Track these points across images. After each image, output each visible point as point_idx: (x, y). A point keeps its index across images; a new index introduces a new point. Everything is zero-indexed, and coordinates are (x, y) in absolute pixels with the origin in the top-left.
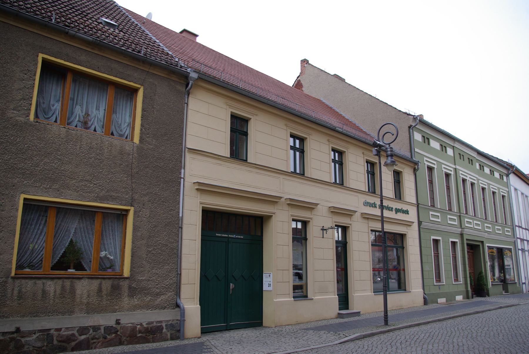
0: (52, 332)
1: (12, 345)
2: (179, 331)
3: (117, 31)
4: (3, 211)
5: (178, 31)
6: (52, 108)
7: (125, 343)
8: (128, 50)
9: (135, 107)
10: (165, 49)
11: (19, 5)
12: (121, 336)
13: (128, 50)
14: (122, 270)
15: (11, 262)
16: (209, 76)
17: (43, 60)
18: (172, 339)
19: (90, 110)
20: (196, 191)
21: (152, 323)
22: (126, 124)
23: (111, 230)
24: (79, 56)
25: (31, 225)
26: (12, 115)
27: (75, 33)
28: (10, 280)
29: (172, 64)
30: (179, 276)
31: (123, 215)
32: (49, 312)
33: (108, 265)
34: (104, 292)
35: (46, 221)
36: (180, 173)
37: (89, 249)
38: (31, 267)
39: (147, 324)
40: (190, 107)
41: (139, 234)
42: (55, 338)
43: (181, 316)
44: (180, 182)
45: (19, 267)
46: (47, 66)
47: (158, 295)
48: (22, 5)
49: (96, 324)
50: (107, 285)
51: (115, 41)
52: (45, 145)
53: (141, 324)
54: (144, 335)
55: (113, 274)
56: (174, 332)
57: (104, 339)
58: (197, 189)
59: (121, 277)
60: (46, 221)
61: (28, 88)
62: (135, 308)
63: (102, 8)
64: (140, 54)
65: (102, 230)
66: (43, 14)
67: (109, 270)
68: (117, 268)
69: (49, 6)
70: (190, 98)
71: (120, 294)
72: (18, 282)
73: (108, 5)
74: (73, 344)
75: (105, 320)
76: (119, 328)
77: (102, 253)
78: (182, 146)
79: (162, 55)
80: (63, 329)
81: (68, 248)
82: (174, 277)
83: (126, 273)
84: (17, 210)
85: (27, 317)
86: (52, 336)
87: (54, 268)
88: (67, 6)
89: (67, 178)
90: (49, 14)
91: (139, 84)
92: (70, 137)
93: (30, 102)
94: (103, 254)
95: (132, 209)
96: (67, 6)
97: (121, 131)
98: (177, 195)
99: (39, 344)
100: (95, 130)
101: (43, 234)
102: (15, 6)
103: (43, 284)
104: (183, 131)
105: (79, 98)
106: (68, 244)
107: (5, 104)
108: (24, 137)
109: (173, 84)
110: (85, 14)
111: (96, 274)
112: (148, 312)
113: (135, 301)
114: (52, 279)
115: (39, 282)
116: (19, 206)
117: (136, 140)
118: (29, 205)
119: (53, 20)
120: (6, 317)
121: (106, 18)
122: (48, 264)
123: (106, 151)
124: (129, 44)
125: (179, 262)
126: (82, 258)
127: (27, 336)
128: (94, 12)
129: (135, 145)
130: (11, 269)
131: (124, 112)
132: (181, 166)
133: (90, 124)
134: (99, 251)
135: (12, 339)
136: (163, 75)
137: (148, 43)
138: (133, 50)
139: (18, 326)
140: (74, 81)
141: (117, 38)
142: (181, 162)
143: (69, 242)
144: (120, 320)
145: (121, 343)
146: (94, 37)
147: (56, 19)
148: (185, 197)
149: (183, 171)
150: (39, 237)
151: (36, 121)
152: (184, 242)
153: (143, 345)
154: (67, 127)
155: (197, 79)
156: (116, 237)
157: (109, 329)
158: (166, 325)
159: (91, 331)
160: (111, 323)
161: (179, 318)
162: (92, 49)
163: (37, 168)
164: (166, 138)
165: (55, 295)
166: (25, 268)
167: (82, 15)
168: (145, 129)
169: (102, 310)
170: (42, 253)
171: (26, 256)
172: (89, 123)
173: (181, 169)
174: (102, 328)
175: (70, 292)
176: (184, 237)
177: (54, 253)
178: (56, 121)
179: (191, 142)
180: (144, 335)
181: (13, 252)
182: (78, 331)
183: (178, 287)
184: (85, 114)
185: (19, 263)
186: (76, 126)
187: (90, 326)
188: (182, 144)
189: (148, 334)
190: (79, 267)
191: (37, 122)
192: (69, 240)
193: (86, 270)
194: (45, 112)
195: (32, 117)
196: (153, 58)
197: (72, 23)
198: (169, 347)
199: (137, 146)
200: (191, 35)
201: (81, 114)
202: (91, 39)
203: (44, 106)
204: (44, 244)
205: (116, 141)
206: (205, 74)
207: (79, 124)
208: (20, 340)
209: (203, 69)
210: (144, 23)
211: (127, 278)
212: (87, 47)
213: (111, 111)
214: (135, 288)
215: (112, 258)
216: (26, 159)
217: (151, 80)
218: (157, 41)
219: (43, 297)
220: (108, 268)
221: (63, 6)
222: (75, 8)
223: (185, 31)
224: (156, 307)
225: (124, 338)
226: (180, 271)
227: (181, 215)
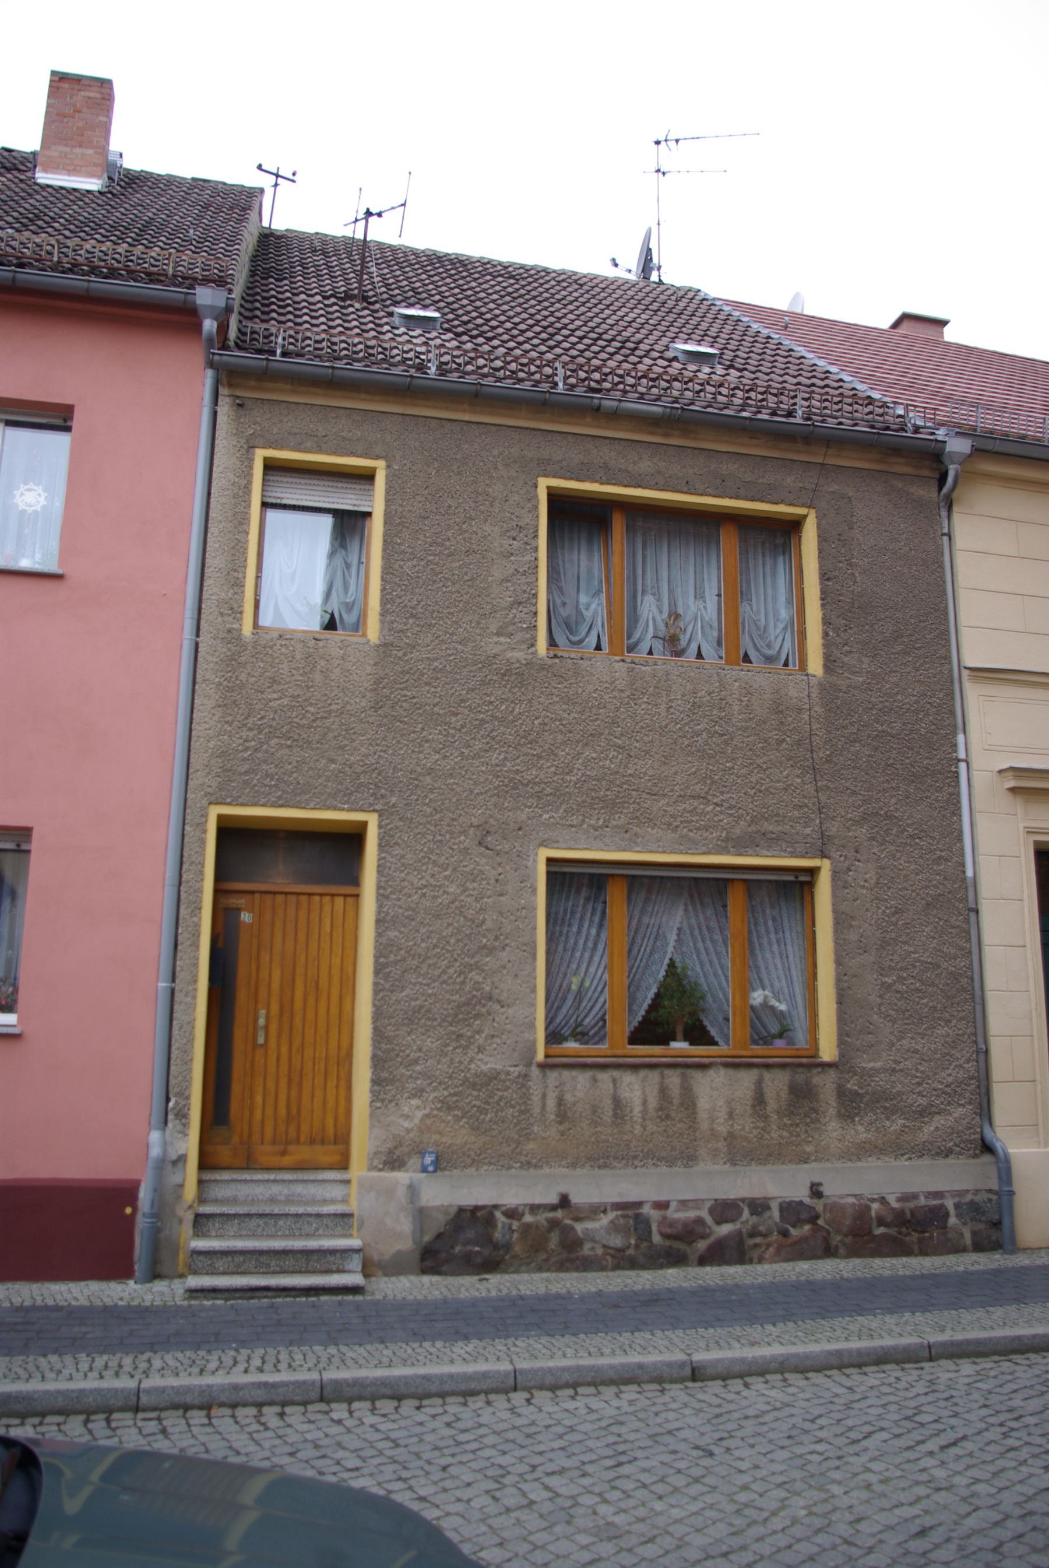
0: (646, 1210)
1: (554, 1239)
2: (997, 1225)
3: (720, 370)
4: (501, 895)
5: (885, 322)
6: (585, 613)
7: (842, 1251)
8: (760, 416)
9: (801, 571)
10: (860, 387)
11: (479, 368)
12: (829, 1233)
13: (760, 416)
14: (815, 1041)
15: (532, 1026)
16: (1005, 438)
17: (549, 495)
18: (979, 1246)
19: (680, 603)
20: (1009, 796)
21: (915, 1196)
22: (781, 626)
23: (772, 929)
24: (635, 463)
25: (570, 925)
26: (496, 650)
27: (615, 403)
28: (535, 1071)
29: (888, 428)
30: (982, 1057)
31: (802, 883)
32: (635, 1157)
33: (774, 1029)
34: (772, 1105)
35: (604, 913)
36: (955, 746)
37: (720, 983)
38: (580, 1035)
39: (899, 1200)
40: (961, 540)
41: (853, 936)
42: (654, 1228)
43: (1000, 1178)
44: (956, 775)
45: (554, 1037)
46: (558, 503)
47: (925, 1113)
48: (485, 366)
49: (757, 1193)
50: (777, 1084)
51: (720, 398)
52: (582, 712)
53: (883, 1200)
54: (893, 1231)
55: (789, 1053)
56: (982, 1226)
57: (781, 1238)
58: (1013, 790)
59: (813, 1063)
60: (604, 913)
61: (524, 574)
62: (861, 1151)
63: (671, 318)
64: (792, 420)
65: (750, 932)
66: (533, 374)
67: (779, 1043)
68: (801, 1038)
69: (543, 348)
70: (956, 517)
71: (816, 1111)
72: (553, 1076)
73: (682, 304)
74: (702, 1245)
75: (781, 1184)
76: (820, 1208)
77: (755, 994)
78: (950, 663)
79: (856, 407)
80: (673, 1205)
81: (663, 985)
82: (968, 1062)
83: (828, 1051)
84: (534, 891)
85: (583, 1166)
86: (647, 1222)
87: (635, 1038)
88: (584, 337)
89: (644, 795)
90: (548, 371)
91: (803, 506)
92: (638, 684)
93: (533, 609)
94: (757, 997)
95: (825, 865)
96: (584, 337)
97: (769, 646)
98: (953, 814)
99: (617, 1241)
100: (699, 656)
101: (601, 947)
102: (468, 373)
103: (614, 1081)
104: (947, 620)
105: (649, 575)
106: (663, 973)
107: (478, 623)
108: (530, 701)
109: (900, 485)
110: (632, 345)
111: (744, 1053)
112: (898, 1163)
113: (861, 1132)
114: (635, 1067)
115: (604, 1077)
116: (536, 880)
117: (815, 665)
118: (564, 878)
119: (561, 385)
120: (536, 1166)
121: (686, 342)
122: (621, 1027)
123: (736, 708)
124: (760, 397)
125: (979, 1014)
126: (703, 1010)
127: (588, 1218)
128: (651, 333)
129: (814, 681)
130: (534, 1043)
131: (770, 592)
132: (955, 726)
133: (683, 643)
134: (745, 989)
135: (554, 1224)
136: (866, 466)
137: (809, 382)
138: (774, 414)
139: (563, 1189)
140: (630, 529)
141: (724, 391)
142: (952, 713)
143: (665, 967)
144: (820, 1184)
145: (829, 1252)
146: (666, 401)
147: (566, 378)
148: (979, 818)
149: (961, 738)
150: (591, 957)
151: (552, 654)
152: (988, 953)
153: (894, 1261)
154: (629, 657)
155: (970, 456)
156: (789, 947)
157: (792, 1211)
158: (957, 1206)
159: (746, 1213)
160: (800, 1193)
161: (994, 1185)
162: (666, 435)
163: (568, 778)
164: (899, 648)
165: (645, 1112)
166: (566, 1039)
167: (623, 351)
168: (836, 630)
169: (770, 1155)
170: (601, 1000)
171: (564, 1010)
172: (682, 637)
173: (955, 734)
174: (775, 1207)
175: (682, 1104)
176: (987, 937)
177: (632, 999)
178: (598, 648)
179: (975, 648)
180: (893, 1231)
181: (535, 999)
182: (711, 1211)
183: (983, 1090)
184: (670, 616)
185: (551, 1028)
186: (650, 653)
187: (743, 1200)
188: (947, 658)
189: (904, 1230)
190: (698, 1035)
191: (555, 656)
192: (666, 961)
193: (716, 1044)
194: (570, 627)
195: (542, 645)
196: (831, 423)
197: (604, 380)
198: (972, 1273)
199: (820, 684)
200: (928, 326)
201: (658, 618)
202: (660, 410)
203: (564, 612)
204: (606, 976)
205: (758, 677)
206: (990, 435)
207: (658, 646)
208: (572, 1228)
209: (985, 421)
210: (786, 327)
211: (829, 1065)
212: (652, 433)
213: (735, 595)
214: (856, 1093)
215: (783, 1007)
216: (540, 757)
217: (835, 487)
218: (833, 369)
219: (615, 1115)
220: (774, 1037)
221: (559, 338)
222: (605, 336)
223: (905, 317)
224: (922, 1151)
225: (836, 1239)
226: (986, 1042)
227: (970, 873)
